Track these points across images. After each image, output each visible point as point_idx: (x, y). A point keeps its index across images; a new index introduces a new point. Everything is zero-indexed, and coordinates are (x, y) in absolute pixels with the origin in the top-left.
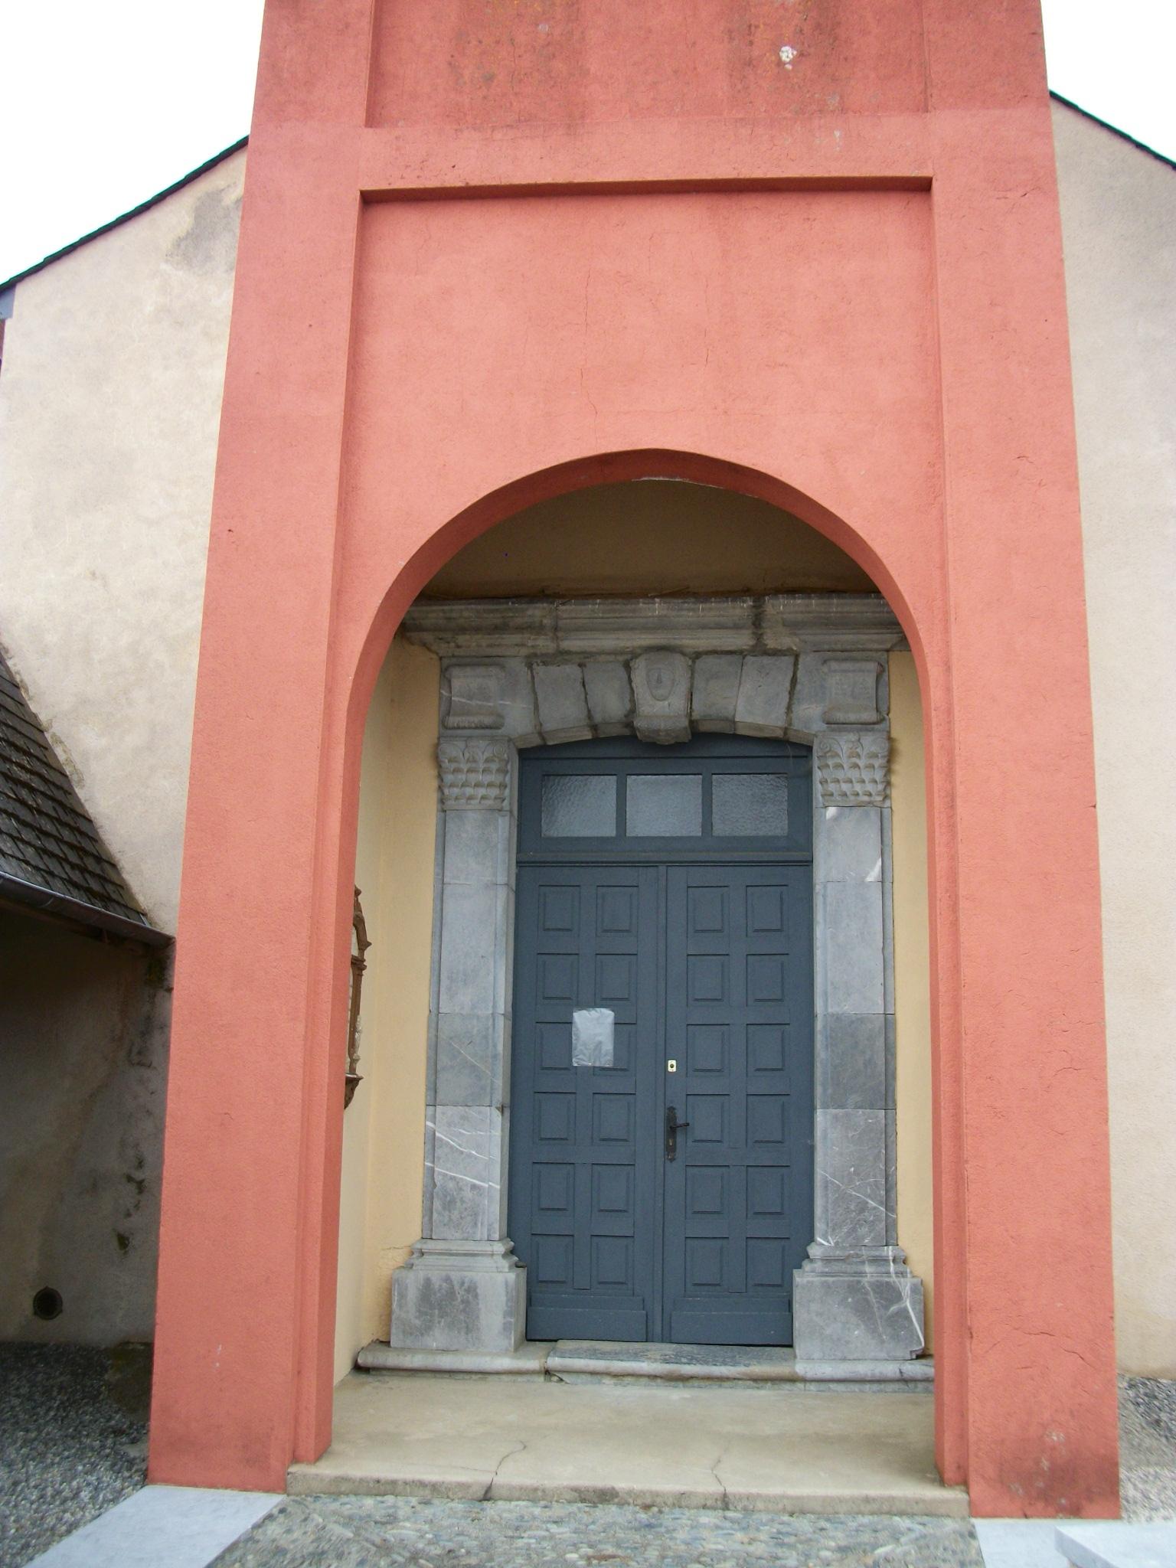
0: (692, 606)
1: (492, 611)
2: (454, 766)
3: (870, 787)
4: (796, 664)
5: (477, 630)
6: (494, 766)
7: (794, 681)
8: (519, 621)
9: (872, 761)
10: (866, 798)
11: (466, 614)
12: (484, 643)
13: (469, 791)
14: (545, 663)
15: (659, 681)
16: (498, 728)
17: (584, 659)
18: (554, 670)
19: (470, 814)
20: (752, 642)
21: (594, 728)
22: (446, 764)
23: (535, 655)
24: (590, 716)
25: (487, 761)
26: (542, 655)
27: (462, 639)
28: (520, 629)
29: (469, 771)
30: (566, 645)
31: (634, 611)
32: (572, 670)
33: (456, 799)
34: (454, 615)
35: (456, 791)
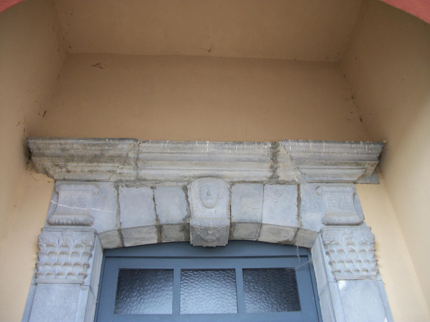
0: (231, 146)
1: (94, 145)
2: (50, 249)
3: (365, 265)
4: (299, 189)
5: (82, 158)
6: (81, 251)
7: (299, 199)
8: (111, 153)
9: (364, 247)
10: (365, 273)
11: (75, 146)
12: (86, 169)
13: (58, 269)
14: (127, 186)
15: (208, 194)
16: (88, 225)
18: (133, 190)
19: (57, 286)
20: (269, 174)
21: (160, 228)
22: (44, 248)
23: (121, 181)
24: (157, 220)
25: (77, 246)
26: (127, 181)
27: (71, 166)
28: (112, 159)
29: (62, 253)
30: (145, 173)
31: (191, 149)
32: (146, 191)
33: (48, 274)
34: (67, 147)
35: (48, 268)
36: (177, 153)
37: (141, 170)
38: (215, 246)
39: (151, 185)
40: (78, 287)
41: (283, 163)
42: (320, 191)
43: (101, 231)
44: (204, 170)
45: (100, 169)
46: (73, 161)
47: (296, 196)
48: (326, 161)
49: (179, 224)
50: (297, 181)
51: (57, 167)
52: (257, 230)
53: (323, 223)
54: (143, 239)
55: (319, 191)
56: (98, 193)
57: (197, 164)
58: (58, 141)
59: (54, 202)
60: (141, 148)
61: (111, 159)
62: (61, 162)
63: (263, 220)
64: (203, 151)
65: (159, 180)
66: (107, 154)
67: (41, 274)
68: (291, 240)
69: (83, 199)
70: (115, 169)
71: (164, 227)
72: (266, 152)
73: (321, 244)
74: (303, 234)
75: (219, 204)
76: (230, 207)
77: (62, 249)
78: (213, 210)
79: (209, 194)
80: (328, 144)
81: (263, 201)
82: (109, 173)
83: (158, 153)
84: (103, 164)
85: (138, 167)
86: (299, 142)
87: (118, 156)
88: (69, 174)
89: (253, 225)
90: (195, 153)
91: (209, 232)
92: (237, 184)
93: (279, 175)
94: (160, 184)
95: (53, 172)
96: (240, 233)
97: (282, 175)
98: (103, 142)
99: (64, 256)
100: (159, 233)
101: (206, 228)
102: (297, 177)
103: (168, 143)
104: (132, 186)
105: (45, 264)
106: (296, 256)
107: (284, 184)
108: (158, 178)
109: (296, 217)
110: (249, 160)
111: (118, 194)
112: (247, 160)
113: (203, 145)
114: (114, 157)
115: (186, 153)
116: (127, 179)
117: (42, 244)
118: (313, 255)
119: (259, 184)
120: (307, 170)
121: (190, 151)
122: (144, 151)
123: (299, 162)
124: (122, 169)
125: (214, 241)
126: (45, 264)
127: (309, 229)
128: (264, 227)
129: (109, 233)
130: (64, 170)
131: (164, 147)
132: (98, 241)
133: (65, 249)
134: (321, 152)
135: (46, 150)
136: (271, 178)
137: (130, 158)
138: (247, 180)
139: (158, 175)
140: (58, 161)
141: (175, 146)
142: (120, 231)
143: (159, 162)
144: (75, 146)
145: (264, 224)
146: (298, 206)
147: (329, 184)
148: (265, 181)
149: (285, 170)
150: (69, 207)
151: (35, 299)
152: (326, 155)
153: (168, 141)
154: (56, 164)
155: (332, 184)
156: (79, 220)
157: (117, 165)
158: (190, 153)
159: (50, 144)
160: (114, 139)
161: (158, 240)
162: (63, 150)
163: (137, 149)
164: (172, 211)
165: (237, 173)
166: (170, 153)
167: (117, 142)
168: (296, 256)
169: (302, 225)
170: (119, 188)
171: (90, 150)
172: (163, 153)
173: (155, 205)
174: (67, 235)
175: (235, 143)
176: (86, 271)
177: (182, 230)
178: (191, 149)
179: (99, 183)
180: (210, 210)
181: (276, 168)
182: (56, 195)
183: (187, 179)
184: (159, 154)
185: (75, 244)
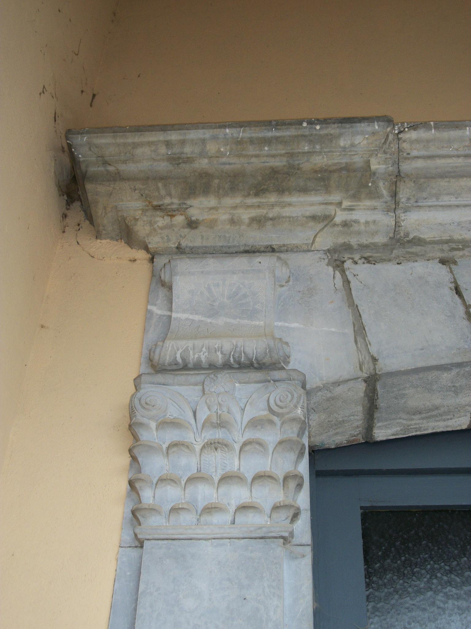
2: (171, 435)
5: (232, 182)
6: (271, 437)
8: (319, 161)
11: (212, 148)
12: (245, 215)
13: (204, 493)
14: (368, 260)
18: (390, 271)
19: (207, 549)
23: (347, 248)
25: (255, 423)
26: (363, 247)
27: (200, 206)
28: (322, 179)
29: (213, 445)
33: (175, 510)
34: (188, 150)
35: (172, 494)
37: (406, 210)
39: (440, 255)
40: (278, 549)
45: (287, 212)
46: (206, 190)
51: (158, 213)
56: (288, 282)
58: (160, 136)
59: (157, 310)
60: (405, 145)
61: (323, 179)
62: (170, 195)
65: (459, 242)
66: (306, 166)
67: (153, 510)
69: (245, 296)
70: (331, 209)
77: (209, 435)
82: (311, 224)
83: (458, 156)
84: (294, 199)
85: (397, 203)
87: (341, 169)
88: (197, 231)
95: (147, 228)
98: (292, 132)
99: (219, 455)
104: (382, 261)
105: (162, 480)
108: (457, 237)
111: (347, 282)
114: (331, 172)
116: (365, 240)
117: (145, 420)
122: (415, 153)
124: (350, 209)
126: (162, 480)
129: (338, 390)
130: (179, 219)
133: (219, 434)
135: (125, 162)
139: (459, 224)
140: (163, 192)
144: (212, 147)
150: (209, 320)
151: (142, 587)
154: (155, 203)
156: (249, 350)
157: (336, 197)
159: (135, 145)
160: (325, 122)
162: (176, 160)
163: (394, 147)
167: (333, 130)
171: (257, 156)
174: (219, 394)
176: (294, 500)
182: (162, 293)
184: (460, 160)
185: (246, 420)
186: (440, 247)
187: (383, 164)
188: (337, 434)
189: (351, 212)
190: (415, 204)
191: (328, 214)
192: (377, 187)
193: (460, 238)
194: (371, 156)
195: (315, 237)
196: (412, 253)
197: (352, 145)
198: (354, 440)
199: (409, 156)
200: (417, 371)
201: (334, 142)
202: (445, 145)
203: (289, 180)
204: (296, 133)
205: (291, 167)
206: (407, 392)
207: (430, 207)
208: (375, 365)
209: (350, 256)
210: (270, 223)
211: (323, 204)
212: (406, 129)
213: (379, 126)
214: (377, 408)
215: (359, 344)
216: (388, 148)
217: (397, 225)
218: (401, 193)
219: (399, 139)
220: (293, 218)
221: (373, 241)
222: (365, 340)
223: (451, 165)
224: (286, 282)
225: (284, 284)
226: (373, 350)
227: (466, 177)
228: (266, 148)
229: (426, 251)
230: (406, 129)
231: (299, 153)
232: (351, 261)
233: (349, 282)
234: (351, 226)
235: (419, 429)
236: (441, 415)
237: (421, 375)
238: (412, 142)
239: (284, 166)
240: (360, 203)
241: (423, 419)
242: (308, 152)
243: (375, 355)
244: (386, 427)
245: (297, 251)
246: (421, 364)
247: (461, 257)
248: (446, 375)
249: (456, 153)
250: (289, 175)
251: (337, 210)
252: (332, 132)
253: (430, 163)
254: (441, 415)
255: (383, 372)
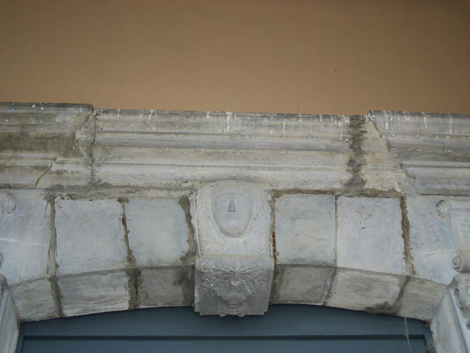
0: (274, 123)
4: (403, 206)
7: (405, 224)
8: (42, 131)
14: (71, 197)
15: (231, 209)
17: (126, 194)
18: (84, 205)
20: (347, 177)
21: (135, 276)
23: (60, 188)
24: (130, 258)
28: (42, 143)
31: (198, 126)
36: (170, 133)
37: (99, 165)
38: (243, 315)
39: (119, 195)
41: (374, 154)
42: (446, 209)
43: (17, 281)
44: (222, 166)
45: (19, 163)
47: (399, 218)
48: (456, 150)
49: (173, 267)
50: (399, 190)
52: (326, 282)
53: (456, 269)
54: (100, 300)
55: (444, 208)
56: (14, 209)
57: (209, 154)
60: (99, 124)
63: (338, 260)
64: (220, 131)
65: (133, 187)
66: (32, 134)
68: (391, 303)
70: (49, 163)
71: (143, 273)
72: (340, 133)
73: (454, 309)
74: (415, 291)
75: (251, 230)
76: (274, 236)
78: (241, 240)
79: (232, 209)
80: (457, 121)
81: (337, 226)
82: (35, 171)
83: (133, 133)
84: (25, 154)
85: (93, 161)
86: (403, 115)
89: (318, 270)
90: (204, 134)
91: (233, 283)
92: (285, 195)
93: (364, 178)
94: (136, 194)
96: (294, 289)
97: (371, 180)
100: (133, 288)
101: (227, 273)
102: (399, 184)
103: (154, 114)
104: (81, 197)
106: (402, 337)
107: (375, 196)
108: (132, 184)
109: (402, 256)
110: (308, 148)
111: (54, 211)
112: (305, 150)
113: (220, 119)
114: (47, 139)
115: (187, 134)
116: (72, 183)
118: (435, 336)
119: (326, 196)
120: (417, 168)
121: (194, 130)
122: (105, 129)
123: (403, 153)
124: (62, 163)
125: (240, 304)
127: (428, 278)
128: (341, 276)
129: (32, 286)
131: (144, 122)
132: (9, 301)
134: (445, 136)
136: (350, 184)
137: (78, 141)
138: (304, 187)
141: (166, 120)
142: (54, 280)
143: (135, 150)
145: (340, 268)
146: (405, 235)
147: (461, 198)
148: (339, 190)
149: (376, 170)
152: (454, 140)
153: (152, 111)
155: (466, 198)
157: (52, 155)
158: (195, 134)
160: (47, 105)
161: (131, 302)
163: (92, 124)
164: (160, 242)
165: (284, 177)
166: (156, 133)
167: (52, 111)
168: (402, 337)
169: (414, 272)
170: (56, 200)
172: (143, 133)
173: (127, 232)
175: (280, 116)
177: (180, 282)
178: (198, 126)
179: (16, 191)
180: (235, 240)
181: (359, 165)
183: (189, 184)
184: (135, 135)
186: (120, 190)
187: (85, 135)
188: (38, 312)
189: (62, 165)
190: (105, 162)
191: (46, 165)
192: (79, 150)
193: (135, 184)
194: (76, 129)
195: (39, 179)
196: (101, 193)
197: (64, 122)
198: (52, 316)
199: (101, 131)
200: (83, 274)
201: (52, 119)
202: (126, 125)
203: (19, 143)
204: (28, 112)
205: (23, 134)
206: (80, 287)
207: (114, 164)
208: (56, 269)
209: (60, 193)
210: (7, 169)
211: (43, 159)
212: (101, 113)
213: (83, 110)
214: (62, 297)
215: (51, 254)
216: (89, 125)
217: (93, 174)
218: (95, 154)
219: (96, 119)
220: (23, 167)
221: (78, 184)
222: (54, 252)
223: (128, 138)
224: (13, 210)
225: (11, 211)
226: (58, 259)
227: (136, 147)
228: (7, 121)
229: (110, 193)
230: (101, 113)
231: (29, 125)
232: (60, 197)
233: (55, 212)
234: (62, 174)
235: (95, 310)
236: (108, 301)
237: (87, 277)
238: (104, 122)
239: (18, 133)
240: (69, 159)
241: (96, 303)
242: (35, 125)
243: (58, 263)
244: (71, 308)
245: (26, 188)
246: (86, 270)
247: (133, 197)
248: (104, 277)
249: (132, 130)
250: (19, 140)
251: (53, 163)
252: (52, 112)
253: (115, 136)
254: (108, 301)
255: (60, 275)
